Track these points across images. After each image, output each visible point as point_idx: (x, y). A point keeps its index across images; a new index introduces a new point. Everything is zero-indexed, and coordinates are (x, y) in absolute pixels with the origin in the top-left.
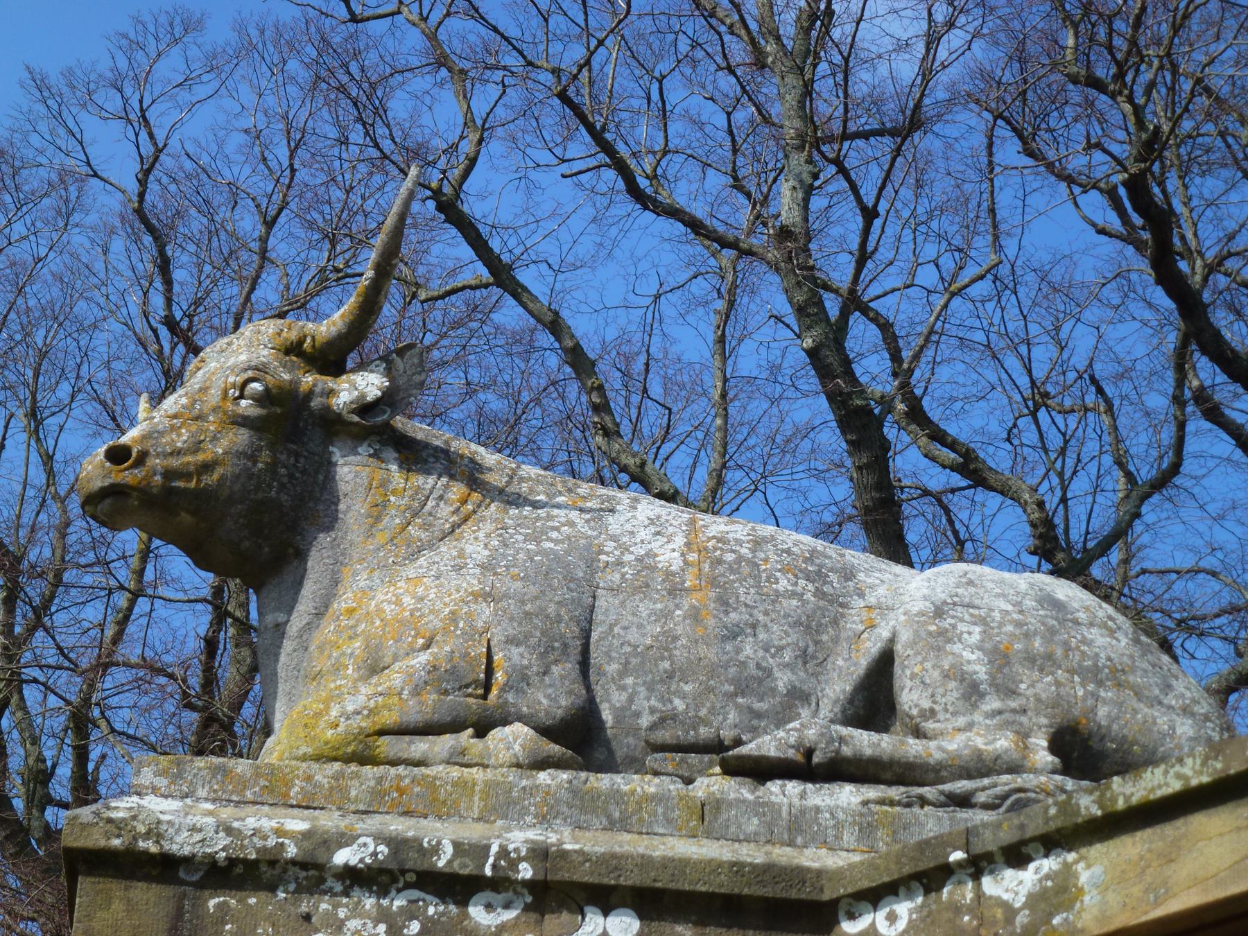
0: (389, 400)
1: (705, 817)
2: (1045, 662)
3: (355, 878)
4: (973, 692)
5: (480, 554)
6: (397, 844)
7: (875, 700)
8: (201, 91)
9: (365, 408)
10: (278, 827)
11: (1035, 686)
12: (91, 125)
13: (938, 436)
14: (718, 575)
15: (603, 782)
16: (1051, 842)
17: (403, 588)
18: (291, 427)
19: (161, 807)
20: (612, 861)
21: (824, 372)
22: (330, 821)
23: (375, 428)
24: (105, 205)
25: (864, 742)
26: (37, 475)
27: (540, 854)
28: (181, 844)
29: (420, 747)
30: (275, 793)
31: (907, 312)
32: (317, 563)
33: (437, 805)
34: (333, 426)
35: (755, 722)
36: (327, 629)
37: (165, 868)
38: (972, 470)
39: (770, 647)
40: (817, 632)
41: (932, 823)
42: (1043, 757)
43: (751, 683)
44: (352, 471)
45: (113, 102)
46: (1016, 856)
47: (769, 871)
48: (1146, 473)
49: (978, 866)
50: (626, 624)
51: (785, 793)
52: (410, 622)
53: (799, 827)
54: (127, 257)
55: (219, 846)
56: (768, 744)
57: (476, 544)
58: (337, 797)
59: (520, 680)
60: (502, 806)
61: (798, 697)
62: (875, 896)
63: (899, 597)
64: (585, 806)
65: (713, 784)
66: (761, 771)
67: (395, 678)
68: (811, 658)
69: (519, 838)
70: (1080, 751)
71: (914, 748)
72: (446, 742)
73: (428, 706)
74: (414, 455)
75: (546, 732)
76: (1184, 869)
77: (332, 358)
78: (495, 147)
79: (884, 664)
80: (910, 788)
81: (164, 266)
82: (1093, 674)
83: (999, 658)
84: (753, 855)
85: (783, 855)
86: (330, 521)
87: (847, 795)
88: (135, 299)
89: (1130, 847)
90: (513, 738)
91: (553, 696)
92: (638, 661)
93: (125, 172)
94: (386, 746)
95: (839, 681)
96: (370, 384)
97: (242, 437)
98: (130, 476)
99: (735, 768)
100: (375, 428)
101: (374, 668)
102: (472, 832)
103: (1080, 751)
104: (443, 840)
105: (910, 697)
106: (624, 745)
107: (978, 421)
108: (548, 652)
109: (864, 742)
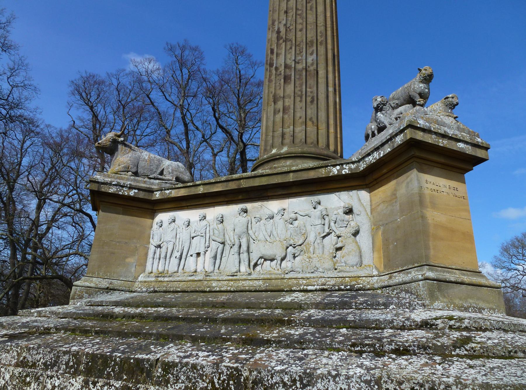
0: (124, 140)
1: (145, 182)
2: (176, 171)
3: (114, 185)
4: (170, 173)
5: (130, 156)
6: (118, 182)
7: (161, 173)
8: (125, 77)
9: (121, 141)
10: (108, 180)
11: (175, 173)
12: (113, 79)
13: (194, 125)
14: (150, 160)
15: (137, 178)
16: (171, 189)
17: (123, 158)
18: (115, 142)
19: (98, 177)
20: (136, 186)
21: (183, 120)
22: (113, 180)
23: (123, 143)
24: (113, 88)
25: (160, 177)
26: (104, 113)
27: (130, 184)
28: (100, 181)
29: (122, 173)
30: (108, 176)
31: (193, 112)
32: (116, 154)
33: (122, 179)
34: (118, 142)
35: (151, 174)
36: (116, 161)
37: (98, 182)
38: (197, 128)
39: (154, 167)
40: (158, 166)
41: (164, 185)
42: (174, 180)
43: (151, 170)
44: (120, 146)
45: (115, 77)
46: (168, 189)
47: (149, 188)
48: (213, 132)
49: (165, 190)
50: (142, 164)
51: (152, 181)
52: (123, 162)
53: (152, 184)
54: (115, 93)
55: (103, 181)
56: (151, 176)
57: (130, 155)
58: (114, 177)
59: (131, 168)
60: (128, 180)
61: (155, 172)
62: (157, 191)
63: (167, 163)
64: (135, 180)
65: (146, 179)
66: (151, 178)
67: (121, 167)
68: (157, 169)
69: (129, 183)
70: (178, 179)
71: (164, 177)
72: (124, 173)
73: (123, 169)
74: (126, 145)
75: (133, 173)
76: (180, 193)
77: (119, 136)
78: (154, 90)
79: (163, 169)
80: (146, 197)
81: (119, 94)
82: (180, 172)
83: (172, 170)
84: (148, 186)
85: (151, 186)
86: (117, 151)
87: (157, 181)
88: (116, 97)
89: (176, 190)
90: (130, 173)
91: (134, 170)
92: (142, 167)
93: (116, 84)
94: (119, 173)
95: (159, 171)
96: (122, 139)
97: (110, 143)
98: (100, 146)
99: (148, 178)
100: (123, 143)
101: (119, 165)
102: (124, 182)
103: (178, 179)
104: (122, 182)
105: (164, 173)
106: (140, 174)
107: (198, 124)
108: (134, 166)
109: (160, 177)
